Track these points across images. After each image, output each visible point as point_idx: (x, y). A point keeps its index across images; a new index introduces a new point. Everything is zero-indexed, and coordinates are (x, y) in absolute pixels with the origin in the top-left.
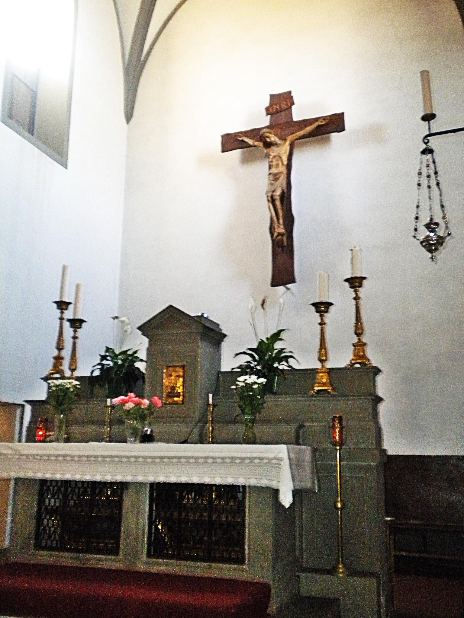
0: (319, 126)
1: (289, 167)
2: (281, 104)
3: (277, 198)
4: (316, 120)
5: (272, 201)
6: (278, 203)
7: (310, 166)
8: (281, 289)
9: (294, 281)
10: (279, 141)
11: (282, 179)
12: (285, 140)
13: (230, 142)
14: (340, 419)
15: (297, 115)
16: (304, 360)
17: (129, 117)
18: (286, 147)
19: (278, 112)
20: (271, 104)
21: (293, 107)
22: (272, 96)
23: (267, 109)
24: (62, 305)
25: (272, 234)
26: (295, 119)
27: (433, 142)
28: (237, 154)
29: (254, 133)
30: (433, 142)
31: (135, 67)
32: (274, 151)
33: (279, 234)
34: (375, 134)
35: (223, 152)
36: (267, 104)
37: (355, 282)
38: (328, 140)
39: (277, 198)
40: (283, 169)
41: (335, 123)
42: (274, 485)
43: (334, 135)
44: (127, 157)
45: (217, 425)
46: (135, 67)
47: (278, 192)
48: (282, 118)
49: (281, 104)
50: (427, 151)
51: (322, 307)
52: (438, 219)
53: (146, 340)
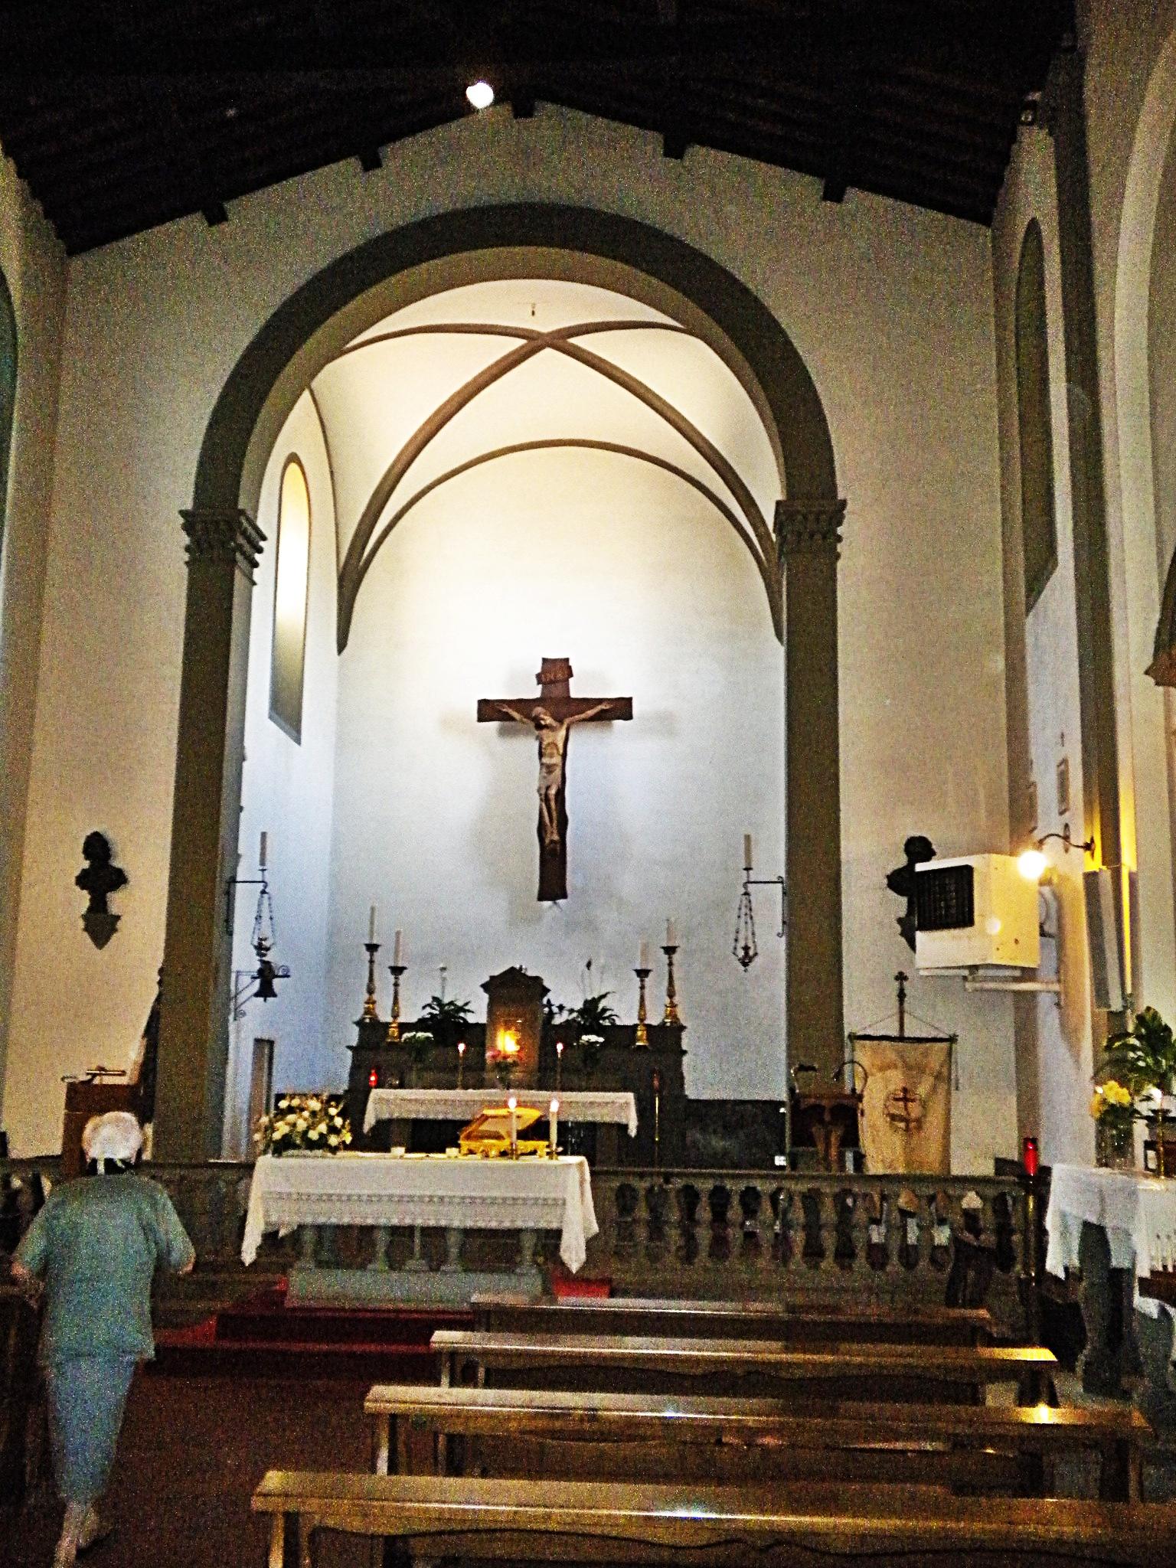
0: (603, 711)
1: (564, 756)
2: (556, 672)
3: (552, 797)
4: (600, 701)
5: (546, 799)
6: (553, 804)
7: (587, 749)
8: (547, 904)
9: (565, 896)
10: (555, 724)
11: (558, 772)
12: (561, 722)
13: (488, 710)
14: (271, 1043)
15: (577, 689)
16: (626, 1017)
17: (342, 645)
18: (563, 732)
19: (552, 682)
20: (544, 671)
21: (571, 680)
22: (545, 660)
23: (538, 676)
24: (372, 948)
25: (541, 839)
26: (573, 694)
27: (751, 888)
28: (494, 725)
29: (522, 705)
30: (751, 888)
31: (351, 579)
32: (548, 737)
33: (552, 841)
34: (666, 725)
35: (480, 720)
36: (539, 670)
37: (670, 950)
38: (610, 726)
39: (552, 797)
40: (557, 760)
41: (622, 709)
42: (624, 1121)
43: (618, 723)
44: (338, 702)
45: (566, 1075)
46: (351, 579)
47: (553, 791)
48: (556, 691)
49: (556, 672)
50: (746, 894)
51: (643, 973)
52: (750, 944)
53: (486, 996)
